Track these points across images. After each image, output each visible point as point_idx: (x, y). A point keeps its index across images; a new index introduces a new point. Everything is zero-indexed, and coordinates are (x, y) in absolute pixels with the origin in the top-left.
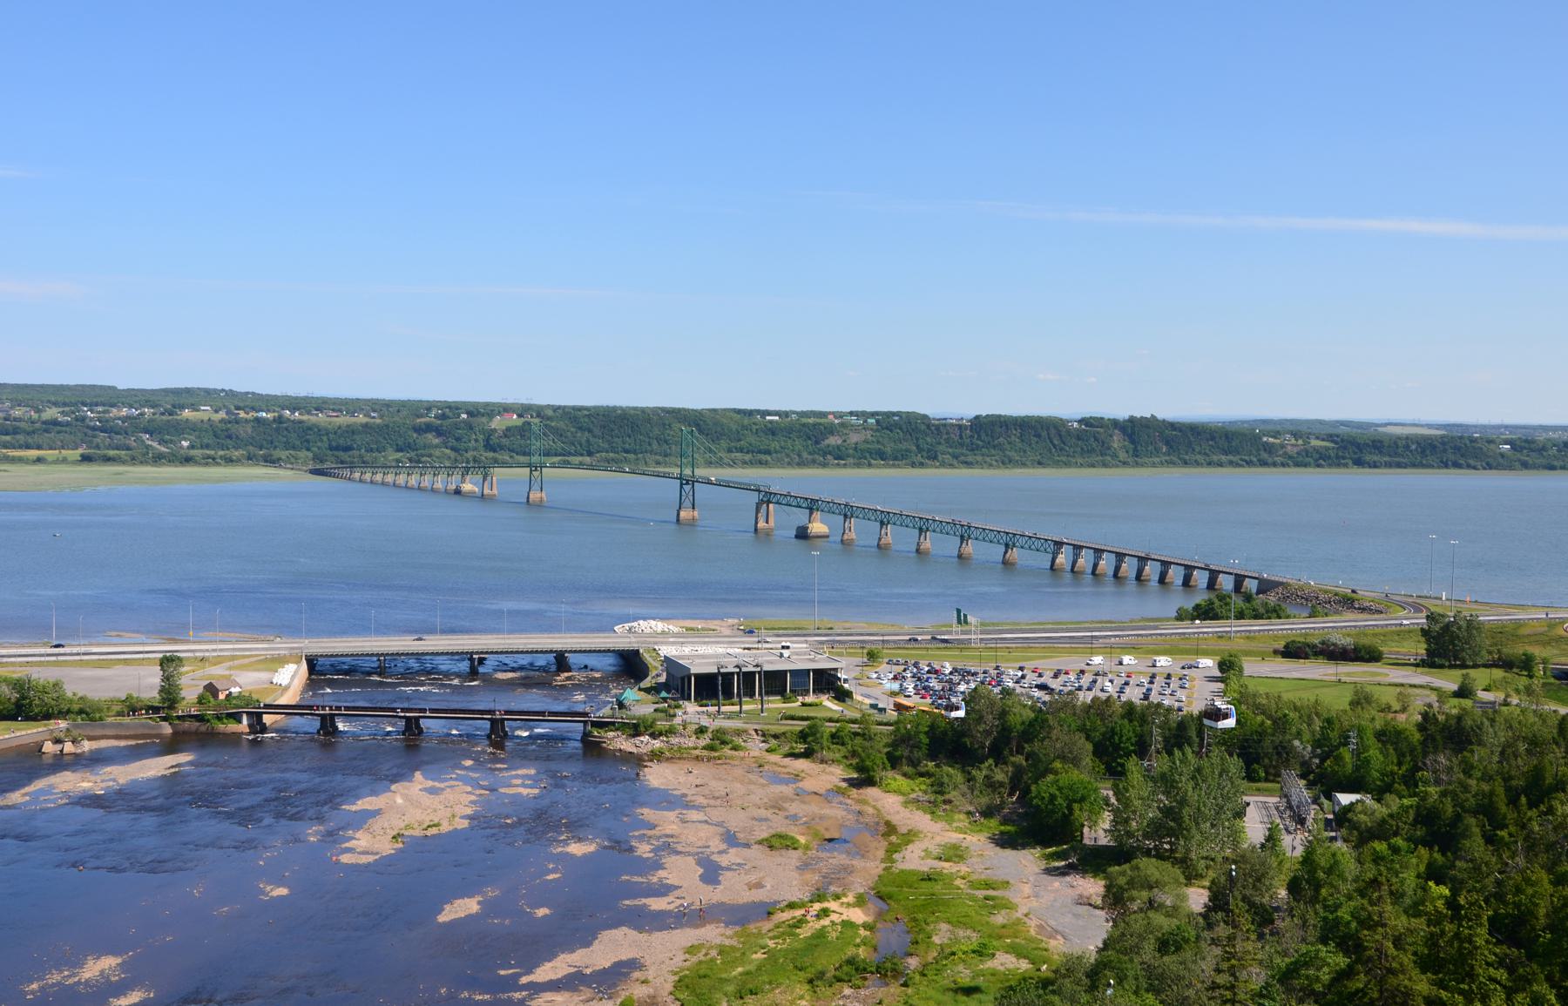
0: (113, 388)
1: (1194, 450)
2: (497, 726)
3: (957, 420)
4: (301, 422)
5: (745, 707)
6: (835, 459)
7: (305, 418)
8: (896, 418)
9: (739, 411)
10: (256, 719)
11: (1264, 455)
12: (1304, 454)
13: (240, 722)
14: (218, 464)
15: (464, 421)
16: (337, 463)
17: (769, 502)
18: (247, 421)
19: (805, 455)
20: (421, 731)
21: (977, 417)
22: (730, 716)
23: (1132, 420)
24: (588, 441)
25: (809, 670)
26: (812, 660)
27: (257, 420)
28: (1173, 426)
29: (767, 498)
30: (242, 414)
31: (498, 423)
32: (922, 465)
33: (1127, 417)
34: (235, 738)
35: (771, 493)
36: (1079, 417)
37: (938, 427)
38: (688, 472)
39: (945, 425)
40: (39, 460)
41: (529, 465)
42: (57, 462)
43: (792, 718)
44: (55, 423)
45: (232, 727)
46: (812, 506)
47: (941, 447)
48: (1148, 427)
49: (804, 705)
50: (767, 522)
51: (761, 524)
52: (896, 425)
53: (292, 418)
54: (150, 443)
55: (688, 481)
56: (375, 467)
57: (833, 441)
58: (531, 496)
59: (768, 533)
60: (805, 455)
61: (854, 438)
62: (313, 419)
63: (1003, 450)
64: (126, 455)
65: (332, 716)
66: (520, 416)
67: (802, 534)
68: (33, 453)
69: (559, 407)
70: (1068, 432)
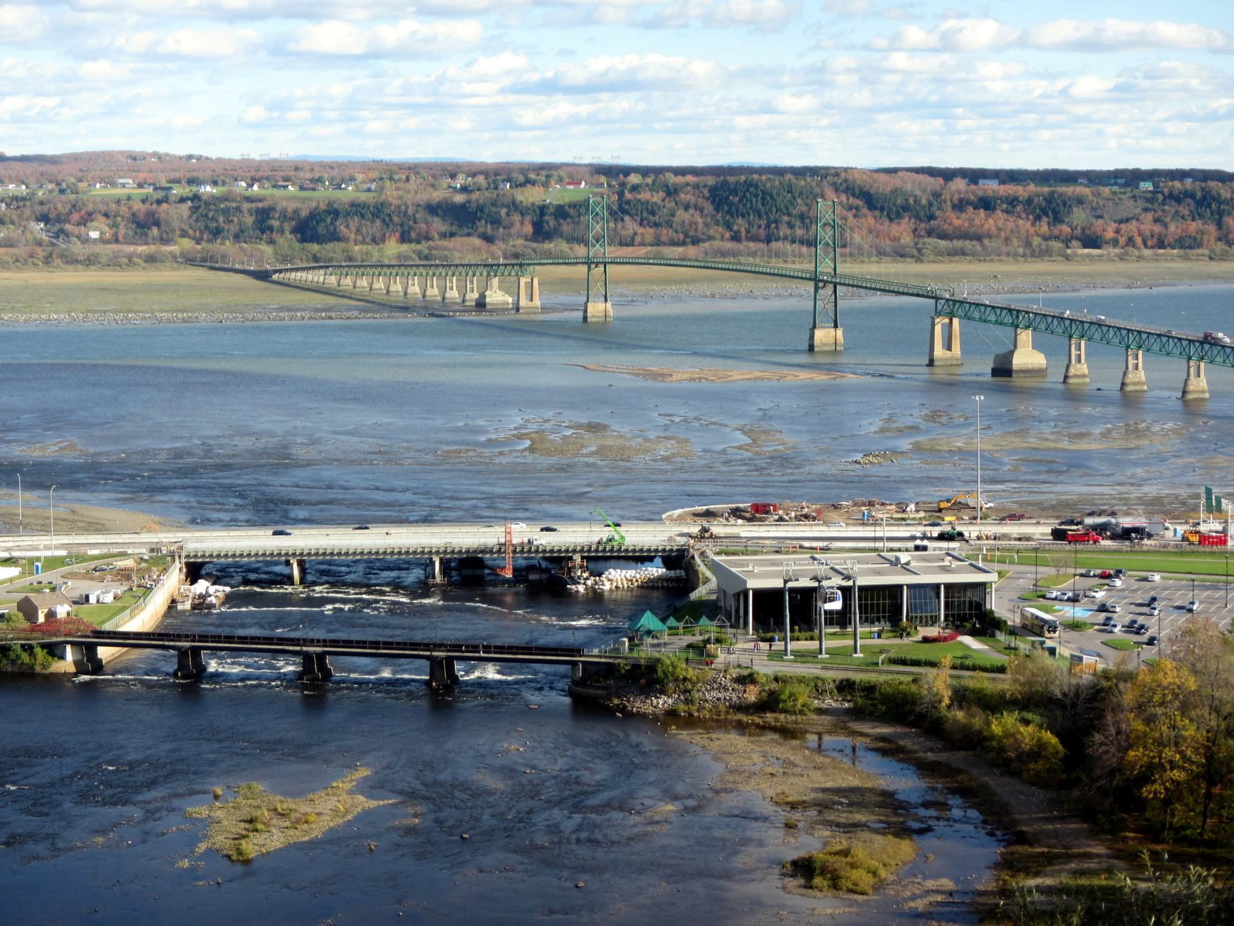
2: (442, 672)
5: (826, 644)
6: (1085, 246)
9: (931, 172)
10: (88, 649)
12: (645, 222)
13: (62, 657)
16: (308, 262)
17: (951, 316)
19: (1036, 241)
20: (327, 675)
22: (800, 656)
26: (945, 570)
35: (955, 302)
38: (825, 267)
41: (589, 263)
43: (903, 662)
46: (1014, 317)
49: (926, 640)
50: (949, 349)
51: (939, 351)
53: (249, 193)
55: (826, 282)
56: (365, 267)
58: (590, 310)
60: (1036, 241)
64: (6, 254)
65: (196, 651)
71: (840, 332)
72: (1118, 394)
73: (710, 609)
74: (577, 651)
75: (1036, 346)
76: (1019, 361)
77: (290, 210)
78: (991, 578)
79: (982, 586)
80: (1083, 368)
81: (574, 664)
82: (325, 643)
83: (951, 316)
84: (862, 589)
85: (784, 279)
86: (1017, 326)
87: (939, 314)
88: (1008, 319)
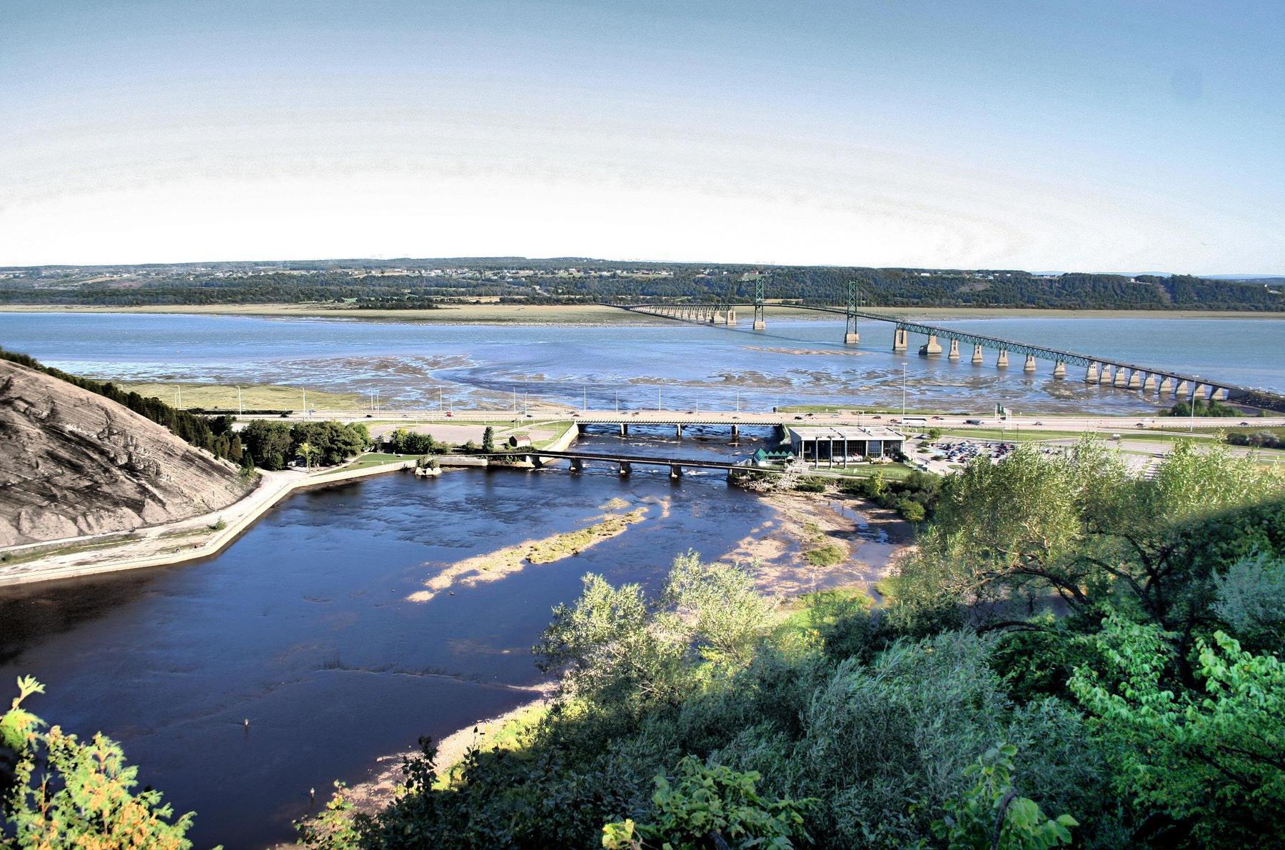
0: (524, 259)
1: (1217, 298)
3: (1051, 276)
4: (626, 277)
7: (630, 274)
8: (1009, 275)
11: (1269, 303)
13: (525, 461)
14: (575, 304)
15: (725, 276)
17: (903, 329)
18: (595, 277)
21: (1066, 274)
23: (1174, 278)
24: (802, 289)
25: (881, 441)
26: (885, 434)
27: (601, 276)
28: (1202, 281)
29: (904, 326)
30: (593, 273)
31: (746, 277)
32: (1022, 307)
33: (1186, 275)
34: (523, 470)
36: (1136, 276)
37: (1035, 281)
39: (1040, 280)
40: (478, 302)
42: (486, 303)
44: (489, 280)
45: (520, 464)
46: (930, 331)
47: (1037, 295)
48: (1183, 282)
51: (898, 344)
52: (1009, 280)
54: (540, 291)
55: (852, 315)
57: (965, 289)
59: (902, 353)
61: (980, 287)
62: (634, 275)
63: (1080, 297)
66: (760, 273)
67: (923, 353)
68: (474, 299)
69: (767, 268)
70: (1128, 286)
71: (857, 335)
72: (1023, 372)
73: (787, 448)
74: (730, 464)
75: (938, 342)
76: (929, 349)
77: (879, 484)
78: (903, 438)
79: (900, 442)
80: (957, 352)
81: (729, 469)
82: (629, 458)
83: (903, 329)
84: (848, 441)
85: (477, 317)
86: (930, 334)
87: (898, 329)
88: (926, 331)
